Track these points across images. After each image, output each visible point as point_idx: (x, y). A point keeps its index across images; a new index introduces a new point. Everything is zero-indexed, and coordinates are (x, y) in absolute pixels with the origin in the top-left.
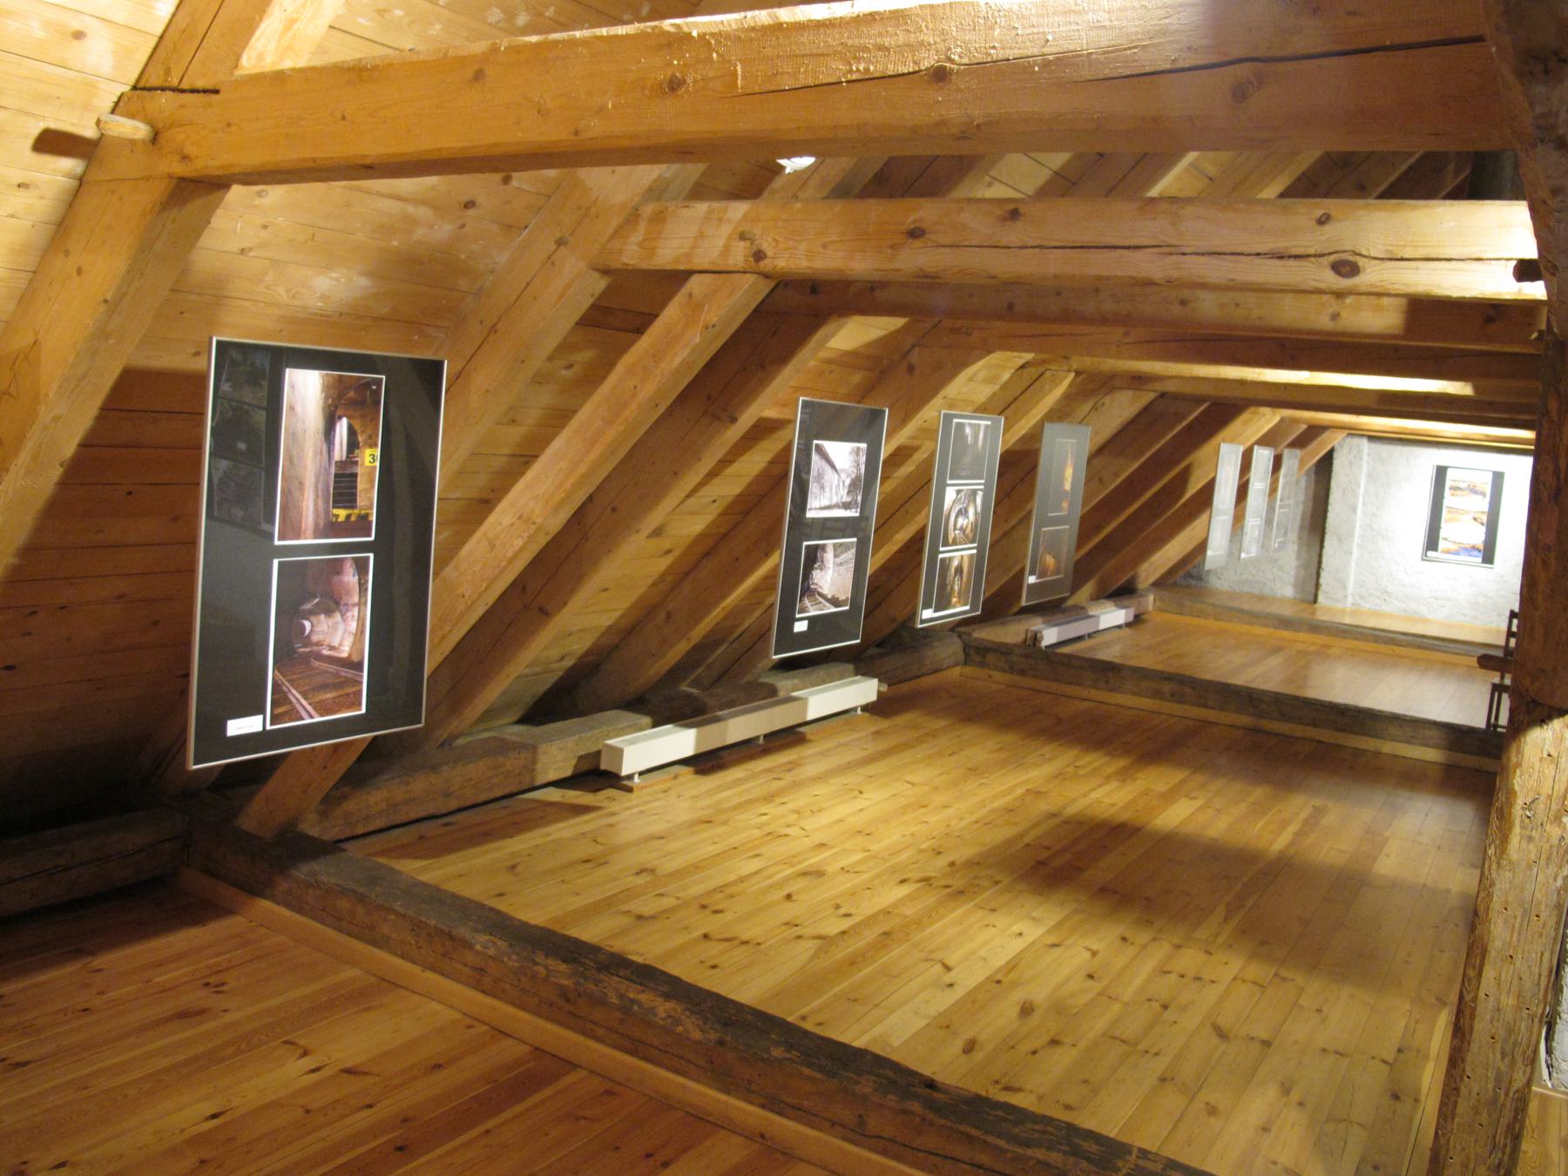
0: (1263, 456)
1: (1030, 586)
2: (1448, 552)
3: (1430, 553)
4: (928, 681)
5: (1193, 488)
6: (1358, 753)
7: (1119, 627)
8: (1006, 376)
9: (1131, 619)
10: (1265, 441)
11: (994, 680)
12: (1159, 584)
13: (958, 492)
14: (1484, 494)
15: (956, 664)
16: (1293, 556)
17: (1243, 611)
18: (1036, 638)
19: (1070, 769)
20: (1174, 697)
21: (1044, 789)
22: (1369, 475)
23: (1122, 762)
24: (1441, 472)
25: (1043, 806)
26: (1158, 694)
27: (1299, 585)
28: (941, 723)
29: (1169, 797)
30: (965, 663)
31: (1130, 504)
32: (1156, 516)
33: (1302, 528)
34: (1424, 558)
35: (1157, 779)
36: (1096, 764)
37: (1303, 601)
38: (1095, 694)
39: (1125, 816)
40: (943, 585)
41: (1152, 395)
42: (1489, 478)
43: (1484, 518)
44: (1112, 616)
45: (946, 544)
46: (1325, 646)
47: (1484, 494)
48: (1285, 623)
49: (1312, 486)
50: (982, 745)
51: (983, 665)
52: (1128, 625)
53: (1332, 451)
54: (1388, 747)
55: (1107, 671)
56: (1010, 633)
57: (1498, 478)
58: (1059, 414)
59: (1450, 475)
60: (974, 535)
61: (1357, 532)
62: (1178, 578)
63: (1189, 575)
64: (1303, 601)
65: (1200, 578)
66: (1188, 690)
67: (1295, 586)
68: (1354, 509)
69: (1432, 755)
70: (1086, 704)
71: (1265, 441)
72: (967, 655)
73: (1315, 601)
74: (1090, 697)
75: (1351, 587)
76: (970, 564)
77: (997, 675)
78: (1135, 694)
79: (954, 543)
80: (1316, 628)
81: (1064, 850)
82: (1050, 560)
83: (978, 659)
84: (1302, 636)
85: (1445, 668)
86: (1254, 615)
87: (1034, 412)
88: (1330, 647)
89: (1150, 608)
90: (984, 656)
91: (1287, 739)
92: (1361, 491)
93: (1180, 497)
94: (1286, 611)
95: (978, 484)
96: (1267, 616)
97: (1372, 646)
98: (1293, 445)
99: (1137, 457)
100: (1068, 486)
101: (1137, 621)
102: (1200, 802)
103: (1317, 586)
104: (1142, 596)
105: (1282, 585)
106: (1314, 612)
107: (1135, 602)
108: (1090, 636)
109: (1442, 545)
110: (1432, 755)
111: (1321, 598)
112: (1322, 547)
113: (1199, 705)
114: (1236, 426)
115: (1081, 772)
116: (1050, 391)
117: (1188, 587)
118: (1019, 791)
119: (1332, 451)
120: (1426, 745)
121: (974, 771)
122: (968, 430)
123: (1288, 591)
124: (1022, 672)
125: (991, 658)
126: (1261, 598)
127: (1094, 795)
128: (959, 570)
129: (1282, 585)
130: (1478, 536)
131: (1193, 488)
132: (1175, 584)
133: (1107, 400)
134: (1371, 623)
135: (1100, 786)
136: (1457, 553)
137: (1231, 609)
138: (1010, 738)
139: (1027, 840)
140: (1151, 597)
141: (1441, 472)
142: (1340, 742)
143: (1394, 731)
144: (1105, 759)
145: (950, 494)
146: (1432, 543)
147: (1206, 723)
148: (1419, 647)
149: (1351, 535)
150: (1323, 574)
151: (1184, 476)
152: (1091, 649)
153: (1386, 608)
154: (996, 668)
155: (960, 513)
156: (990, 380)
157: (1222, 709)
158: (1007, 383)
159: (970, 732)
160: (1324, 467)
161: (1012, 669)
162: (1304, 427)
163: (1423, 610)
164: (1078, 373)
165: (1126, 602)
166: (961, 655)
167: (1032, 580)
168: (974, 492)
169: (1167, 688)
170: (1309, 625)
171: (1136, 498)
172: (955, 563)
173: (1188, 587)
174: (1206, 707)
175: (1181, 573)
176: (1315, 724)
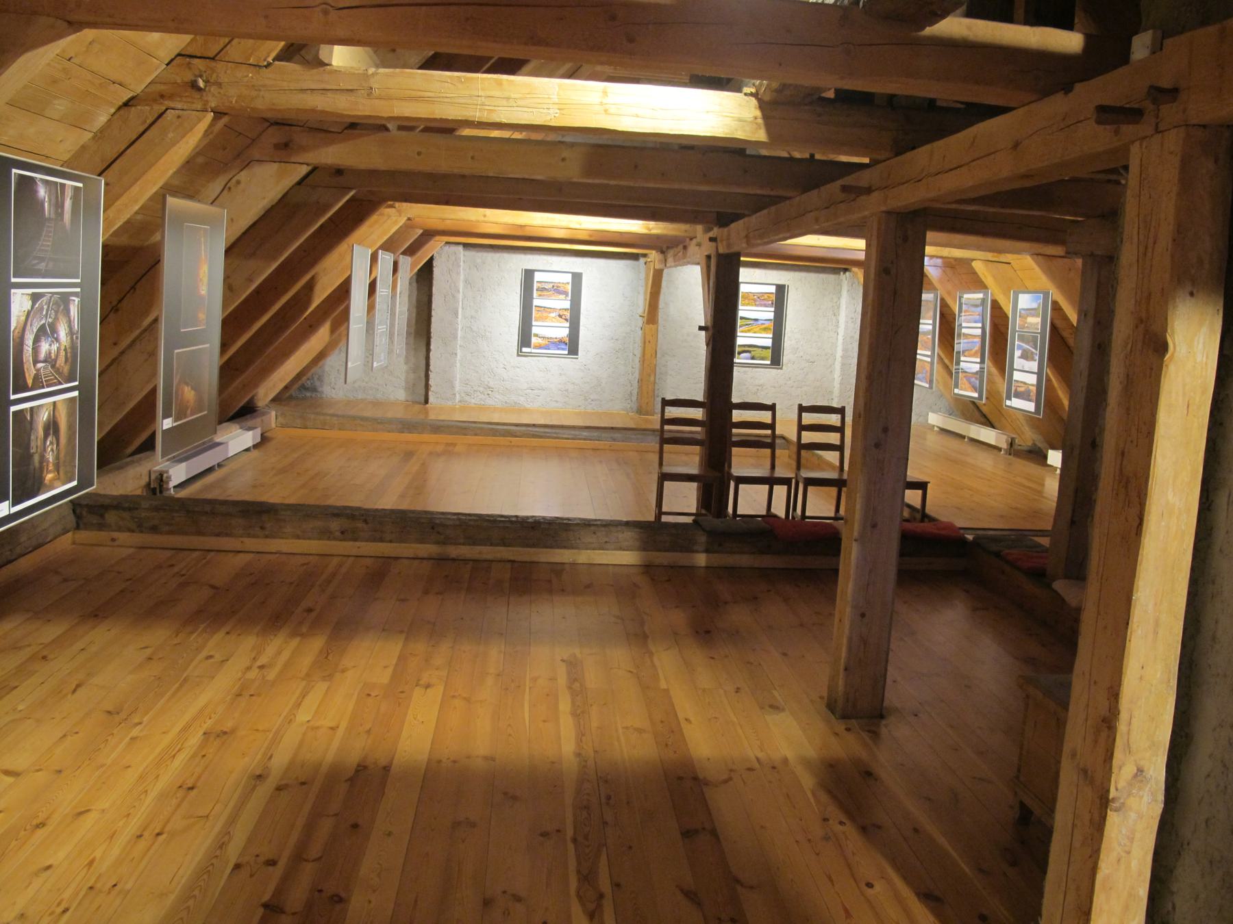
0: (386, 259)
1: (165, 432)
2: (540, 347)
3: (524, 350)
4: (24, 565)
5: (320, 295)
6: (558, 569)
7: (247, 450)
8: (103, 119)
9: (259, 440)
10: (388, 246)
11: (118, 545)
12: (276, 400)
13: (35, 298)
14: (566, 293)
15: (65, 532)
16: (402, 360)
17: (363, 419)
18: (161, 479)
19: (252, 675)
20: (345, 535)
21: (228, 725)
22: (466, 281)
23: (317, 643)
24: (529, 275)
25: (237, 763)
26: (326, 534)
27: (411, 388)
28: (52, 631)
29: (397, 692)
30: (78, 527)
31: (257, 318)
32: (282, 329)
33: (408, 333)
34: (520, 353)
35: (371, 660)
36: (286, 655)
37: (415, 402)
38: (251, 543)
39: (357, 750)
40: (24, 458)
41: (304, 170)
42: (568, 278)
43: (568, 314)
44: (238, 439)
45: (21, 386)
46: (447, 444)
47: (566, 293)
48: (407, 426)
49: (415, 293)
50: (118, 658)
51: (101, 527)
52: (255, 446)
53: (431, 259)
54: (584, 557)
55: (257, 514)
56: (128, 481)
57: (577, 278)
58: (198, 174)
59: (538, 277)
60: (72, 367)
61: (460, 334)
62: (292, 392)
63: (304, 388)
64: (415, 402)
65: (314, 390)
66: (360, 525)
67: (406, 389)
68: (456, 314)
69: (627, 558)
70: (241, 560)
71: (388, 246)
72: (78, 517)
73: (426, 401)
74: (243, 550)
75: (458, 386)
76: (71, 415)
77: (122, 537)
78: (298, 537)
79: (38, 383)
80: (438, 428)
81: (299, 857)
82: (189, 394)
83: (95, 520)
84: (426, 437)
85: (561, 453)
86: (362, 420)
87: (150, 175)
88: (454, 445)
89: (273, 425)
90: (102, 516)
91: (478, 565)
92: (461, 296)
93: (306, 309)
94: (399, 413)
95: (71, 285)
96: (390, 421)
97: (489, 440)
98: (404, 253)
99: (275, 259)
100: (203, 291)
101: (264, 440)
102: (437, 692)
103: (427, 387)
104: (264, 414)
105: (394, 389)
106: (427, 413)
107: (258, 420)
108: (219, 465)
109: (534, 340)
110: (627, 558)
111: (431, 399)
112: (428, 350)
113: (374, 540)
114: (362, 230)
115: (271, 675)
116: (174, 143)
117: (304, 398)
118: (195, 739)
119: (431, 259)
120: (621, 549)
121: (116, 715)
122: (42, 192)
123: (401, 395)
124: (154, 529)
125: (111, 517)
126: (376, 404)
127: (303, 716)
128: (52, 427)
129: (394, 389)
130: (563, 332)
131: (320, 295)
132: (291, 397)
133: (243, 176)
134: (484, 418)
135: (304, 696)
136: (547, 347)
137: (354, 418)
138: (158, 635)
139: (233, 853)
140: (273, 413)
141: (529, 275)
142: (535, 559)
143: (588, 538)
144: (295, 642)
145: (20, 303)
146: (525, 339)
147: (388, 561)
148: (534, 436)
149: (455, 338)
150: (431, 375)
151: (310, 287)
152: (224, 479)
153: (490, 402)
154: (120, 529)
155: (41, 333)
156: (76, 123)
157: (401, 541)
158: (102, 130)
159: (100, 635)
160: (425, 275)
161: (140, 527)
162: (421, 231)
163: (522, 400)
164: (218, 114)
165: (250, 423)
166: (71, 519)
167: (168, 423)
168: (65, 298)
169: (335, 525)
170: (426, 427)
171: (265, 310)
172: (44, 416)
173: (304, 398)
174: (381, 540)
175: (296, 386)
176: (504, 543)
